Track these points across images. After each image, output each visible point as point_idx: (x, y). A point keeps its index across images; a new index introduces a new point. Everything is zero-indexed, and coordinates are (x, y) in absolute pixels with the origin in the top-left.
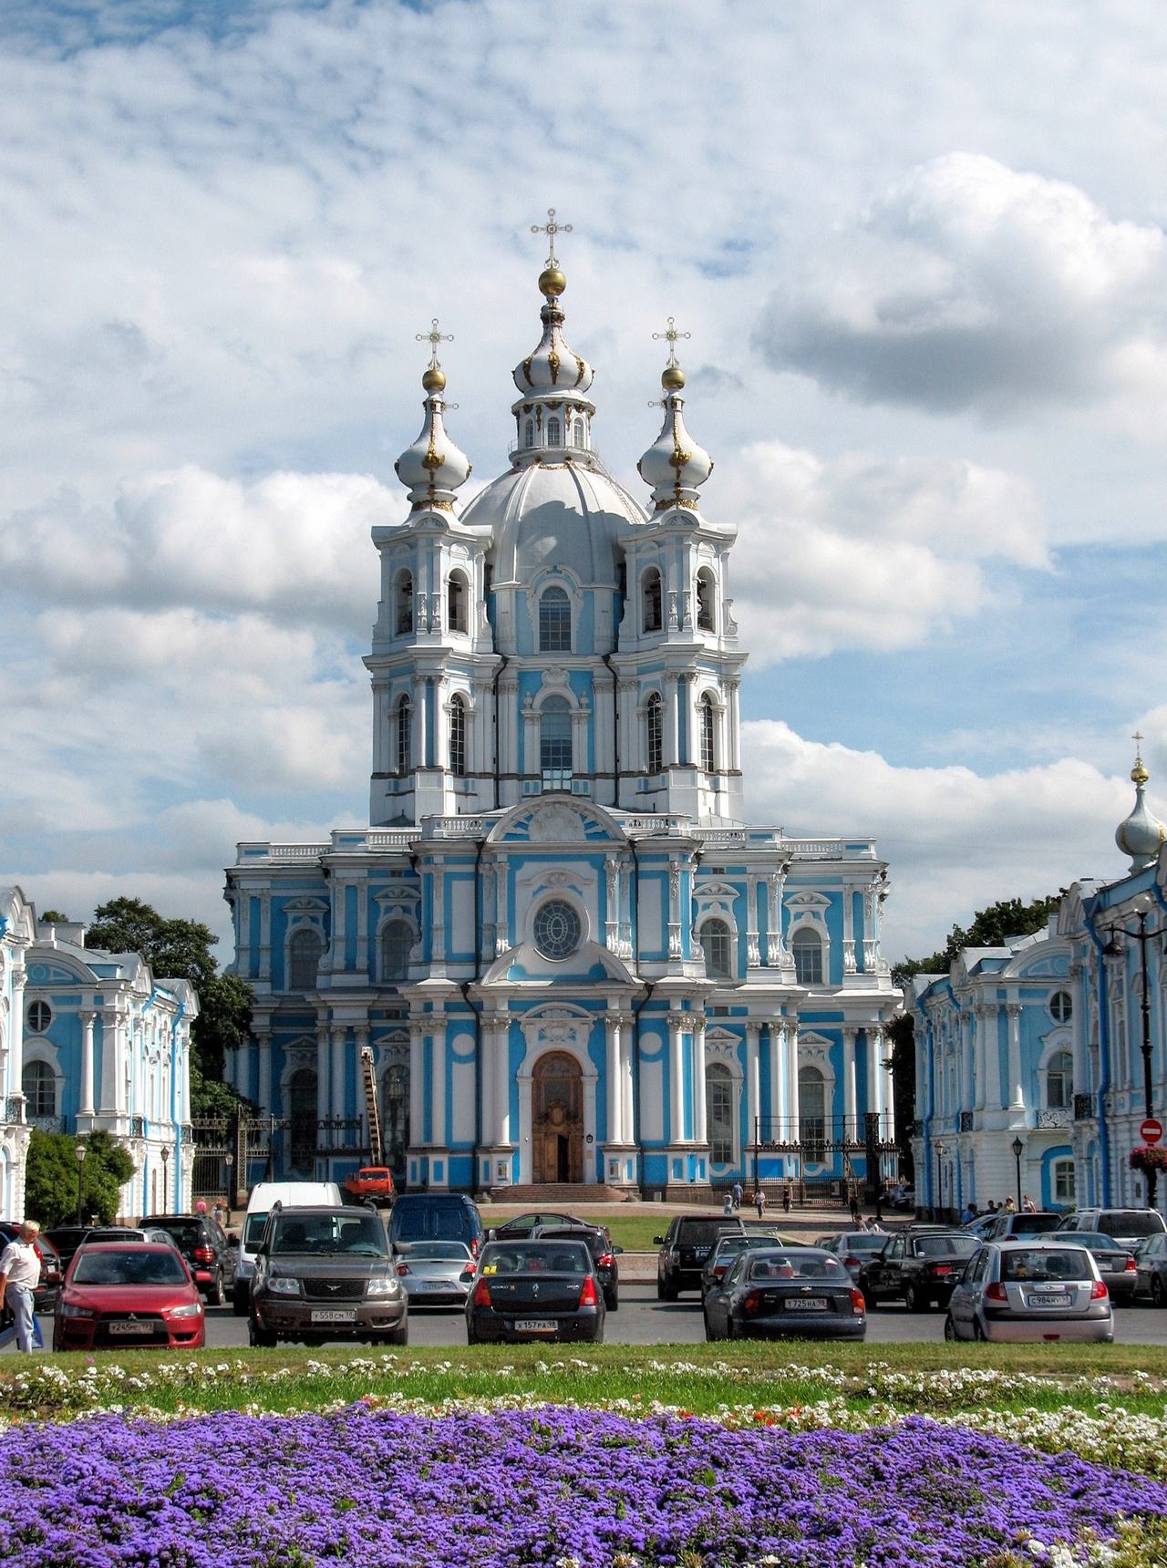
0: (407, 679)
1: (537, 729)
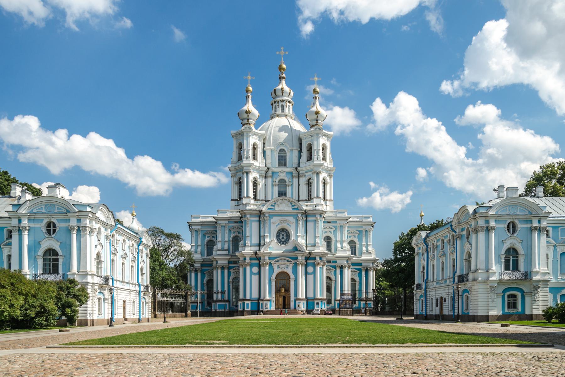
0: (241, 173)
1: (277, 188)
